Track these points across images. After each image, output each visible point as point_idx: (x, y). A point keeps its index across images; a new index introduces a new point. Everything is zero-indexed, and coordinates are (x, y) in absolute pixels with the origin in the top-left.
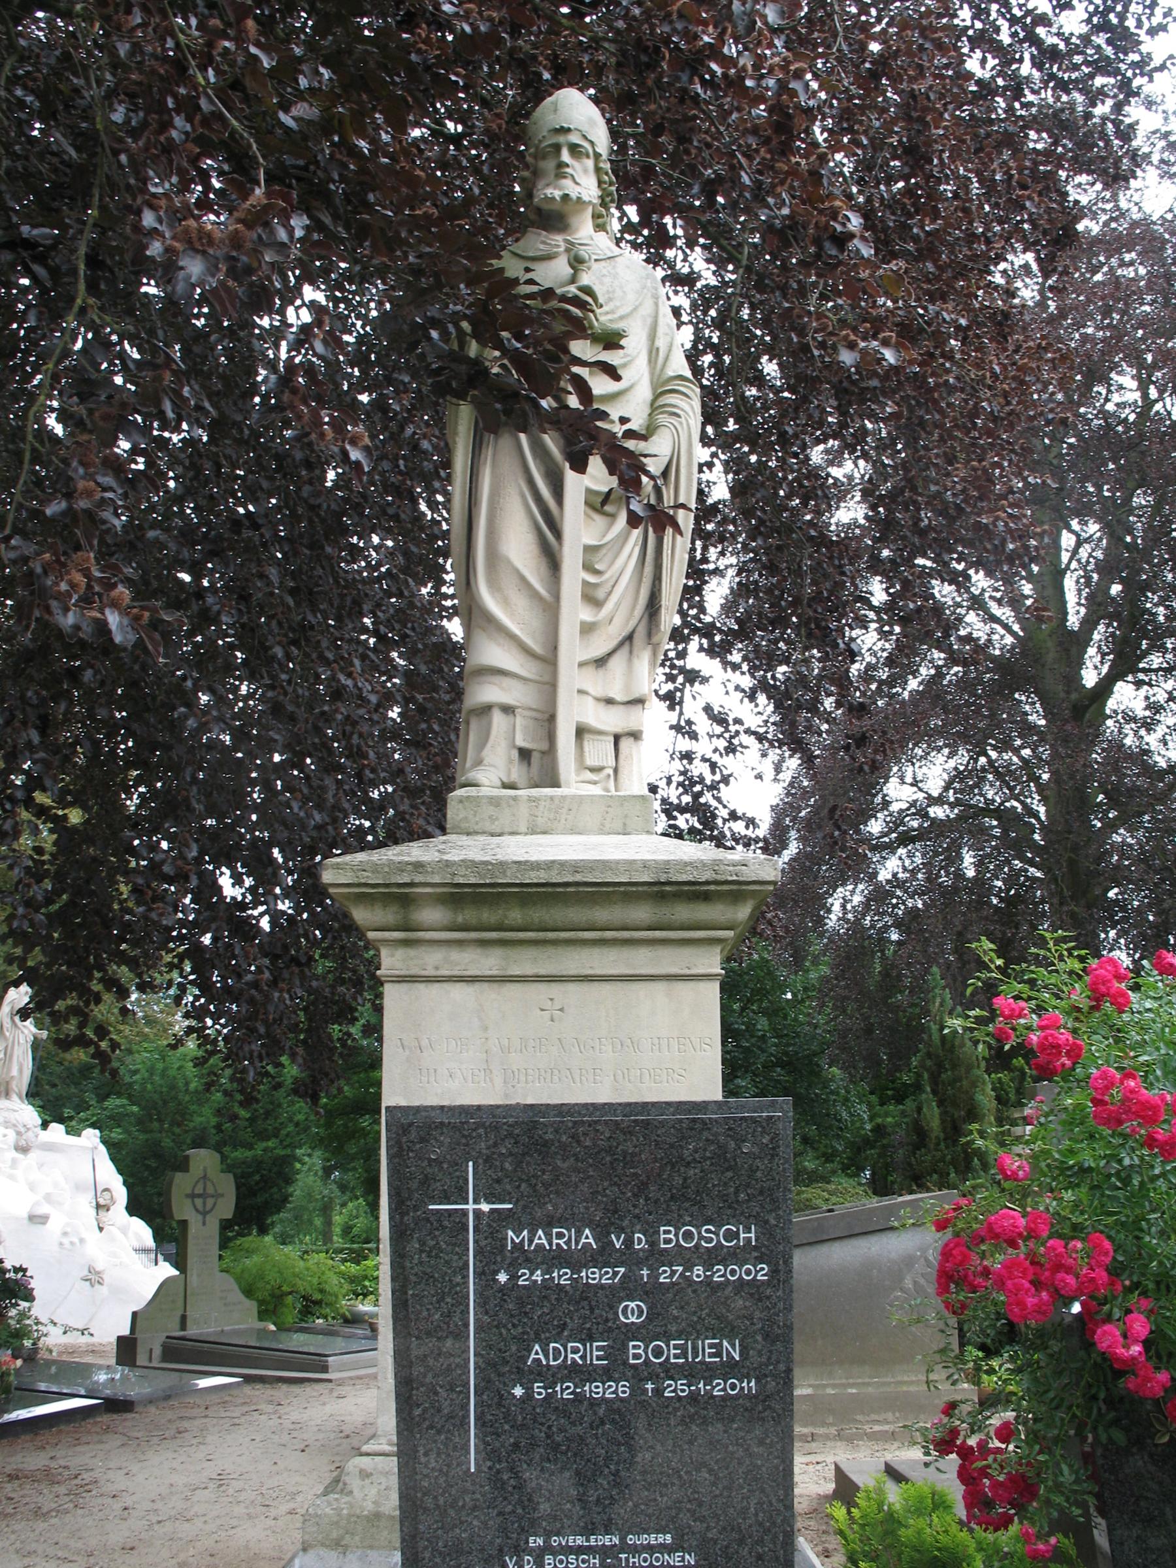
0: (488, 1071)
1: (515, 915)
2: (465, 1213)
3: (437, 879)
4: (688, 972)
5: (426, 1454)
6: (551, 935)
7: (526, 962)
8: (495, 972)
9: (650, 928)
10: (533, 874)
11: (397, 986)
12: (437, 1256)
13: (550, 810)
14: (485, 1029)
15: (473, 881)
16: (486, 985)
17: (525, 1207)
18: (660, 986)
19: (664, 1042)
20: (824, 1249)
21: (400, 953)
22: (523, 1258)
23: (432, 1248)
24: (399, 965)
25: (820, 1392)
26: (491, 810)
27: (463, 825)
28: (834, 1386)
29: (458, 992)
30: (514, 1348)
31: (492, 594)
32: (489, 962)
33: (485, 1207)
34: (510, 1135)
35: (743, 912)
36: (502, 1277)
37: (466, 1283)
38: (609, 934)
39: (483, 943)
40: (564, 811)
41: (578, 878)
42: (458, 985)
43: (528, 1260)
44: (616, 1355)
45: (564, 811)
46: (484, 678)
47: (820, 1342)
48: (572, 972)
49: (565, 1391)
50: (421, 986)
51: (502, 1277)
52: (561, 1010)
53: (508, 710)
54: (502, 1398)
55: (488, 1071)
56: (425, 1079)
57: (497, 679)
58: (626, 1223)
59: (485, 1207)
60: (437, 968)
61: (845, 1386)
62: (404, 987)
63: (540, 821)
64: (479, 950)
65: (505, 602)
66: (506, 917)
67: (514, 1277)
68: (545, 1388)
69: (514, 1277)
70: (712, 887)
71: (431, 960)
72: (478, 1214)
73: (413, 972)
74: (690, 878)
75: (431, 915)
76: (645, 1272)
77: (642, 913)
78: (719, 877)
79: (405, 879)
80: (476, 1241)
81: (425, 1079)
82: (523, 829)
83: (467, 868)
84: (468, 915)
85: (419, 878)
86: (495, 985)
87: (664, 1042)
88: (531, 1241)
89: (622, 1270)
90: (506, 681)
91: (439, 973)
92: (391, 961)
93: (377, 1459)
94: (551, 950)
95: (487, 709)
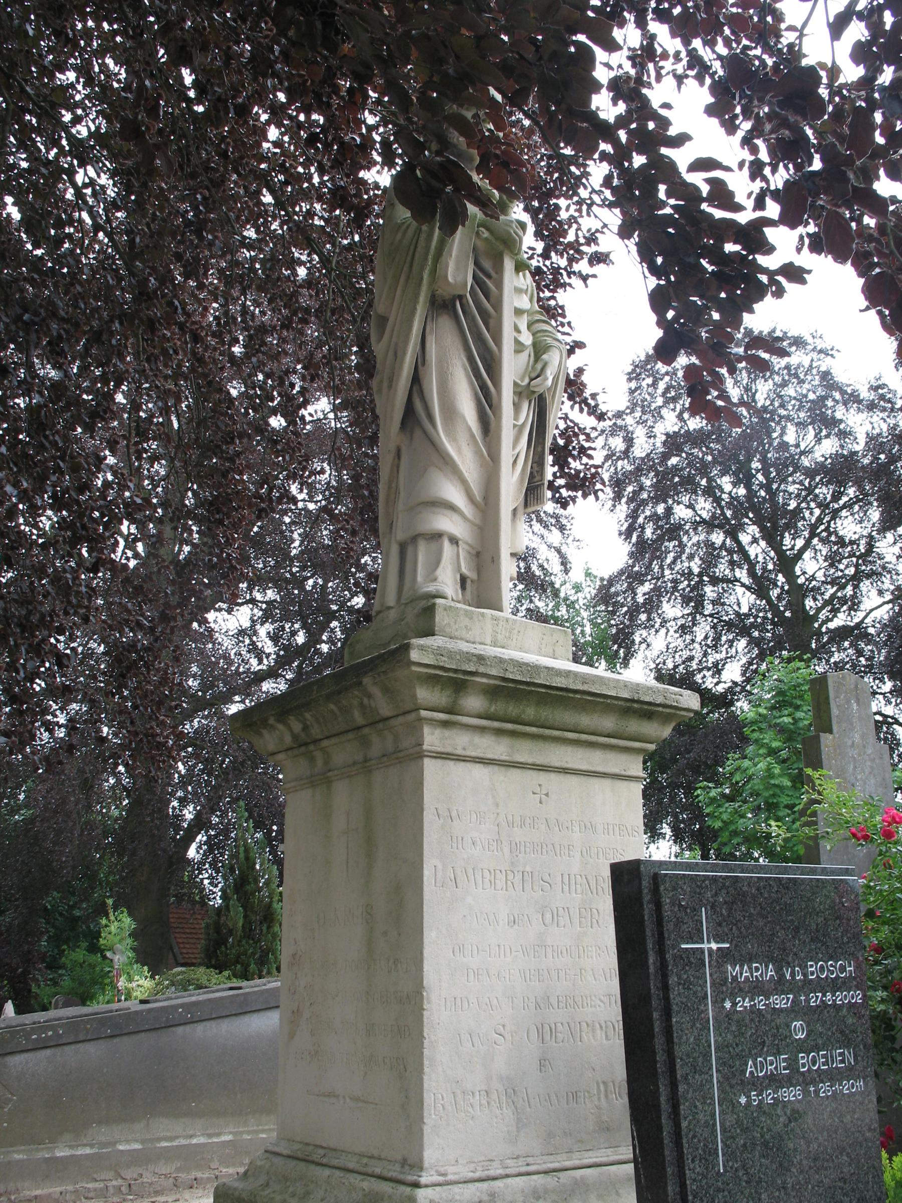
0: (499, 841)
1: (530, 712)
2: (702, 951)
3: (494, 672)
4: (623, 773)
5: (693, 1161)
6: (547, 732)
7: (526, 752)
8: (503, 758)
9: (608, 736)
10: (558, 679)
11: (433, 760)
12: (689, 989)
13: (506, 629)
14: (497, 805)
15: (518, 678)
16: (496, 768)
17: (736, 946)
18: (607, 782)
19: (611, 827)
20: (246, 1019)
21: (438, 732)
22: (739, 989)
23: (685, 980)
24: (437, 742)
25: (238, 1137)
26: (467, 621)
27: (448, 630)
28: (248, 1133)
29: (479, 772)
30: (738, 1063)
31: (449, 442)
32: (498, 748)
33: (714, 946)
34: (724, 886)
35: (666, 732)
36: (728, 1005)
37: (707, 1010)
38: (584, 737)
39: (499, 732)
40: (516, 631)
41: (585, 688)
42: (478, 765)
43: (741, 990)
44: (792, 1064)
45: (516, 631)
46: (437, 510)
47: (239, 1096)
48: (557, 764)
49: (769, 1097)
50: (451, 763)
51: (728, 1005)
52: (547, 795)
53: (454, 541)
54: (734, 1105)
55: (499, 841)
56: (455, 845)
57: (449, 513)
58: (790, 959)
59: (714, 946)
60: (464, 749)
61: (257, 1132)
62: (439, 762)
63: (500, 637)
64: (493, 738)
65: (459, 451)
66: (524, 712)
67: (734, 1004)
68: (757, 1095)
69: (734, 1004)
70: (660, 709)
71: (461, 741)
72: (710, 950)
73: (449, 749)
74: (651, 700)
75: (474, 702)
76: (803, 998)
77: (608, 723)
78: (667, 702)
79: (471, 668)
80: (711, 975)
81: (455, 845)
82: (488, 641)
83: (514, 666)
84: (498, 707)
85: (482, 669)
86: (503, 769)
87: (611, 827)
88: (741, 974)
89: (791, 996)
90: (456, 517)
91: (468, 753)
92: (432, 738)
93: (535, 1177)
94: (541, 744)
95: (438, 536)
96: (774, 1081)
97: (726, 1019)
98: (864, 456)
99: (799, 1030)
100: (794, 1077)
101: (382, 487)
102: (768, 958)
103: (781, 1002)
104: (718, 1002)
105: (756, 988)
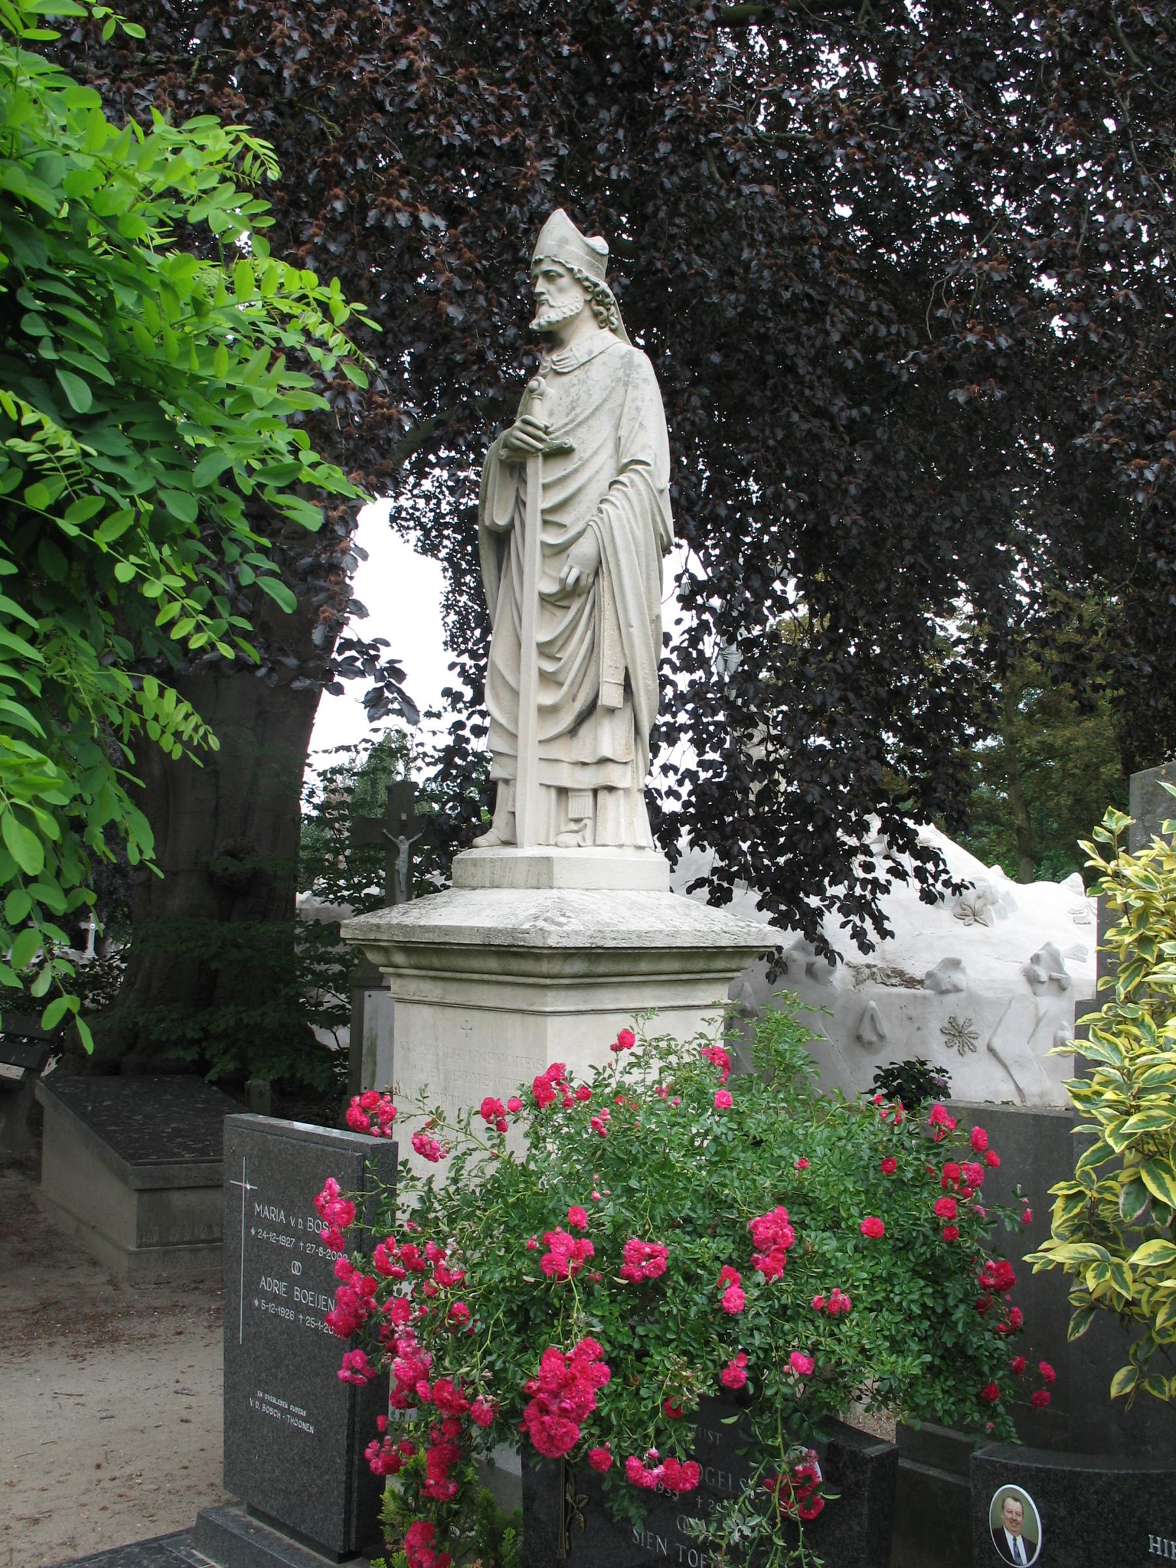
6: (458, 975)
7: (455, 994)
29: (426, 1011)
32: (433, 991)
44: (290, 1291)
94: (465, 986)
96: (275, 1298)
97: (253, 1241)
98: (1034, 586)
99: (296, 1267)
100: (288, 1302)
101: (552, 821)
102: (281, 1206)
103: (284, 1241)
104: (248, 1228)
105: (271, 1226)
